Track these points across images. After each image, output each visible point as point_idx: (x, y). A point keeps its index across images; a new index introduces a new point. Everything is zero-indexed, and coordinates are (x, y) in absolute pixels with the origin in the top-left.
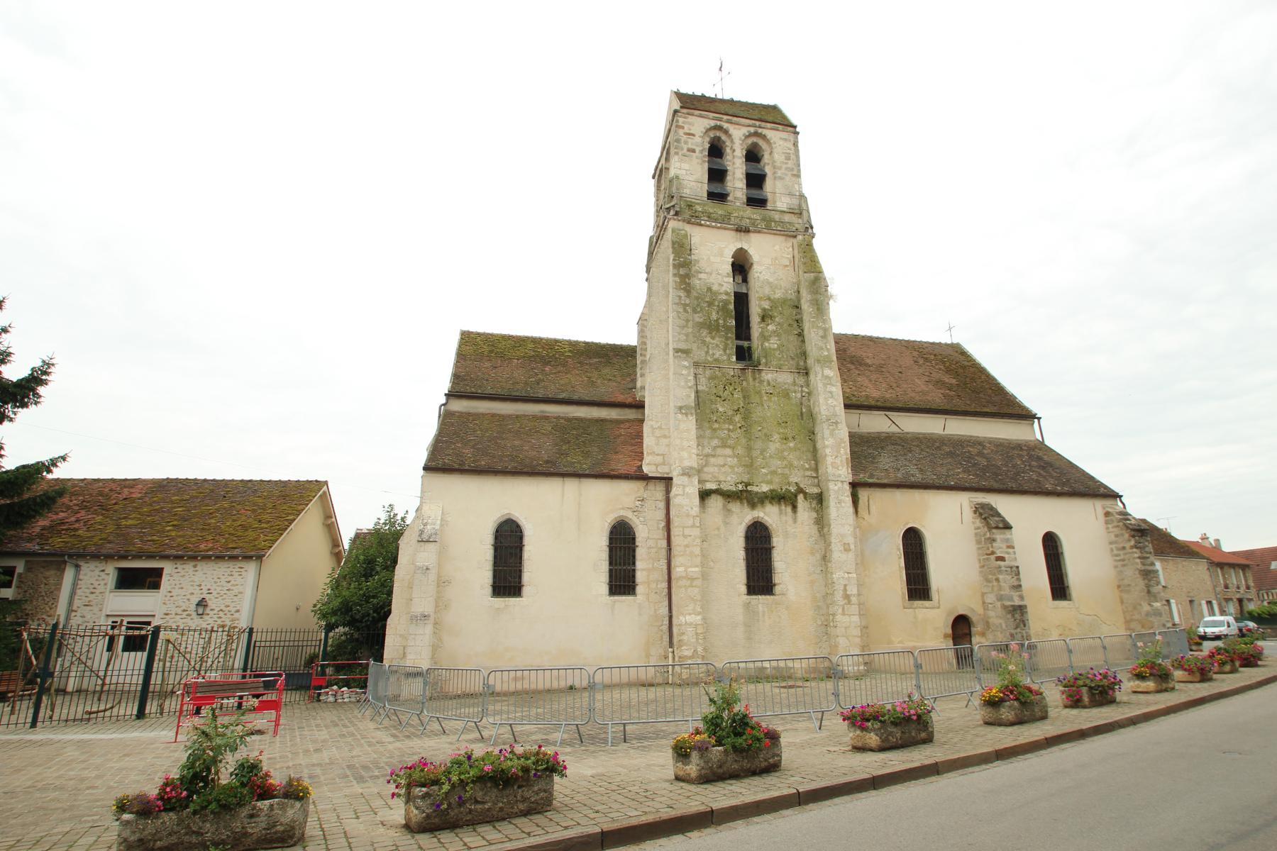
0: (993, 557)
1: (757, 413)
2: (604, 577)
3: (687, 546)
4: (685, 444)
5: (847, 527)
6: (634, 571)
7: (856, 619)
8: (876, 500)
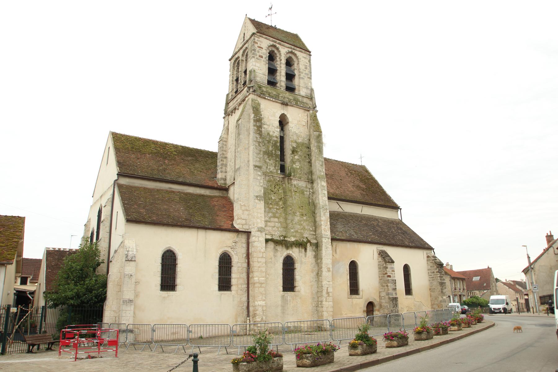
0: (386, 275)
1: (290, 201)
2: (216, 282)
3: (259, 267)
4: (259, 215)
5: (329, 260)
6: (230, 278)
7: (331, 303)
8: (341, 246)
